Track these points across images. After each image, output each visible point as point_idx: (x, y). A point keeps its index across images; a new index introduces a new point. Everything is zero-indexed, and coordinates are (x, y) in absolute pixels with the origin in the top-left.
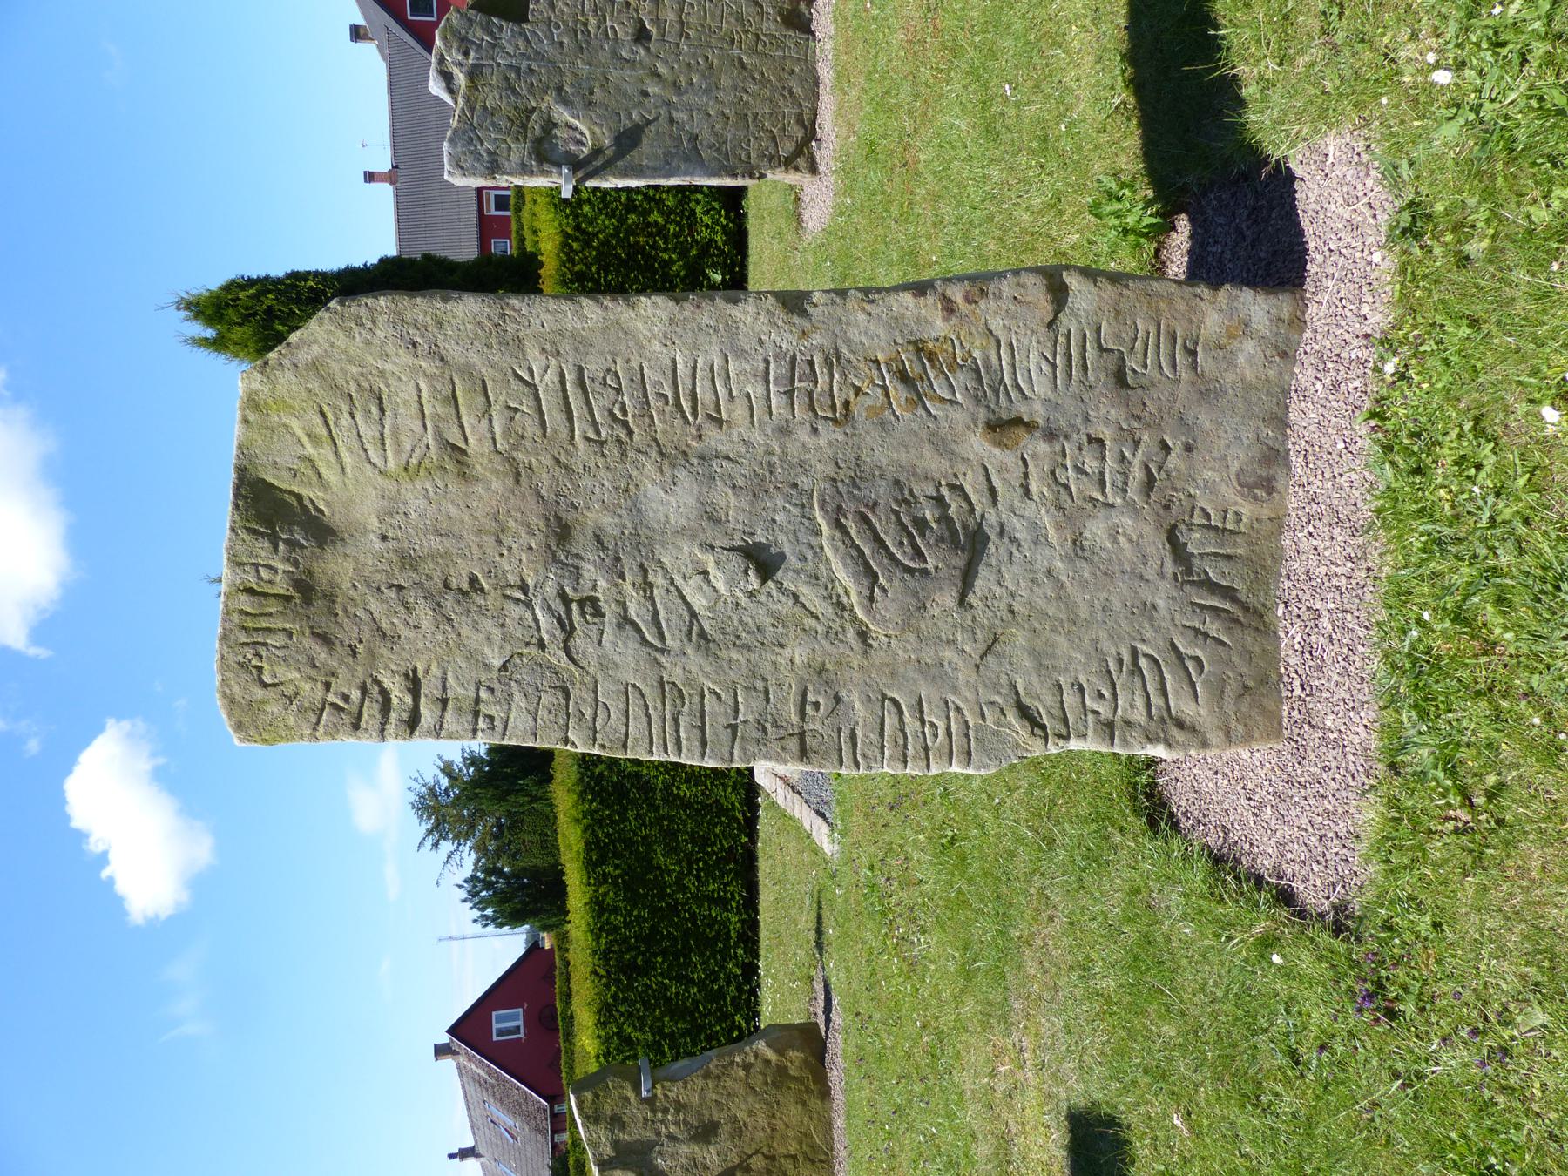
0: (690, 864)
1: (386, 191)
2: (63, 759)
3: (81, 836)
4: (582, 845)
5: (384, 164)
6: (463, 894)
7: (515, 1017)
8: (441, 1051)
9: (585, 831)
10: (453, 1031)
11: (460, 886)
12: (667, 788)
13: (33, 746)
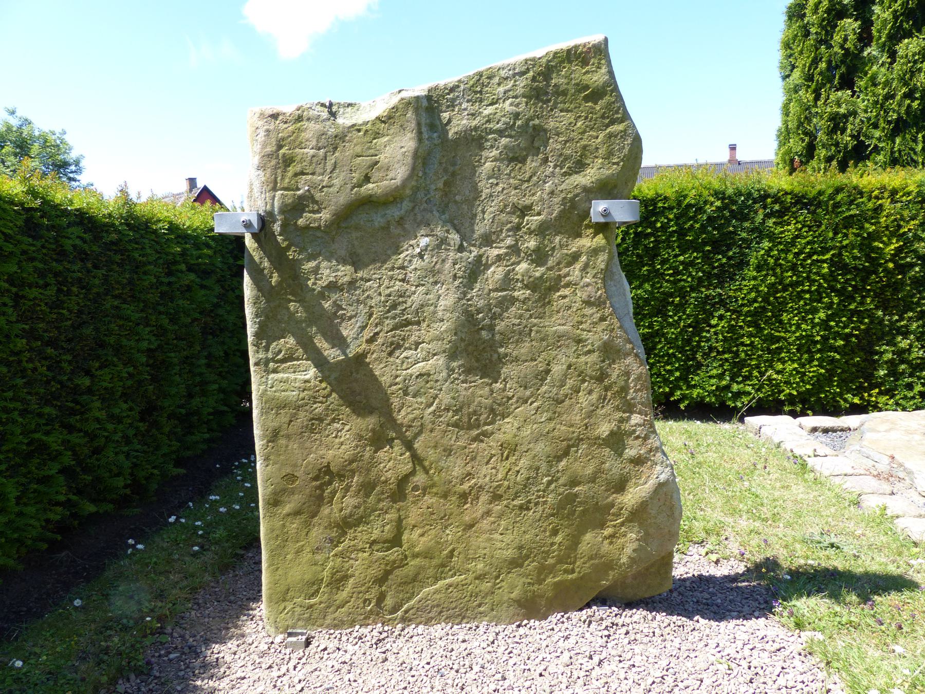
1: (723, 156)
5: (741, 156)
8: (192, 182)
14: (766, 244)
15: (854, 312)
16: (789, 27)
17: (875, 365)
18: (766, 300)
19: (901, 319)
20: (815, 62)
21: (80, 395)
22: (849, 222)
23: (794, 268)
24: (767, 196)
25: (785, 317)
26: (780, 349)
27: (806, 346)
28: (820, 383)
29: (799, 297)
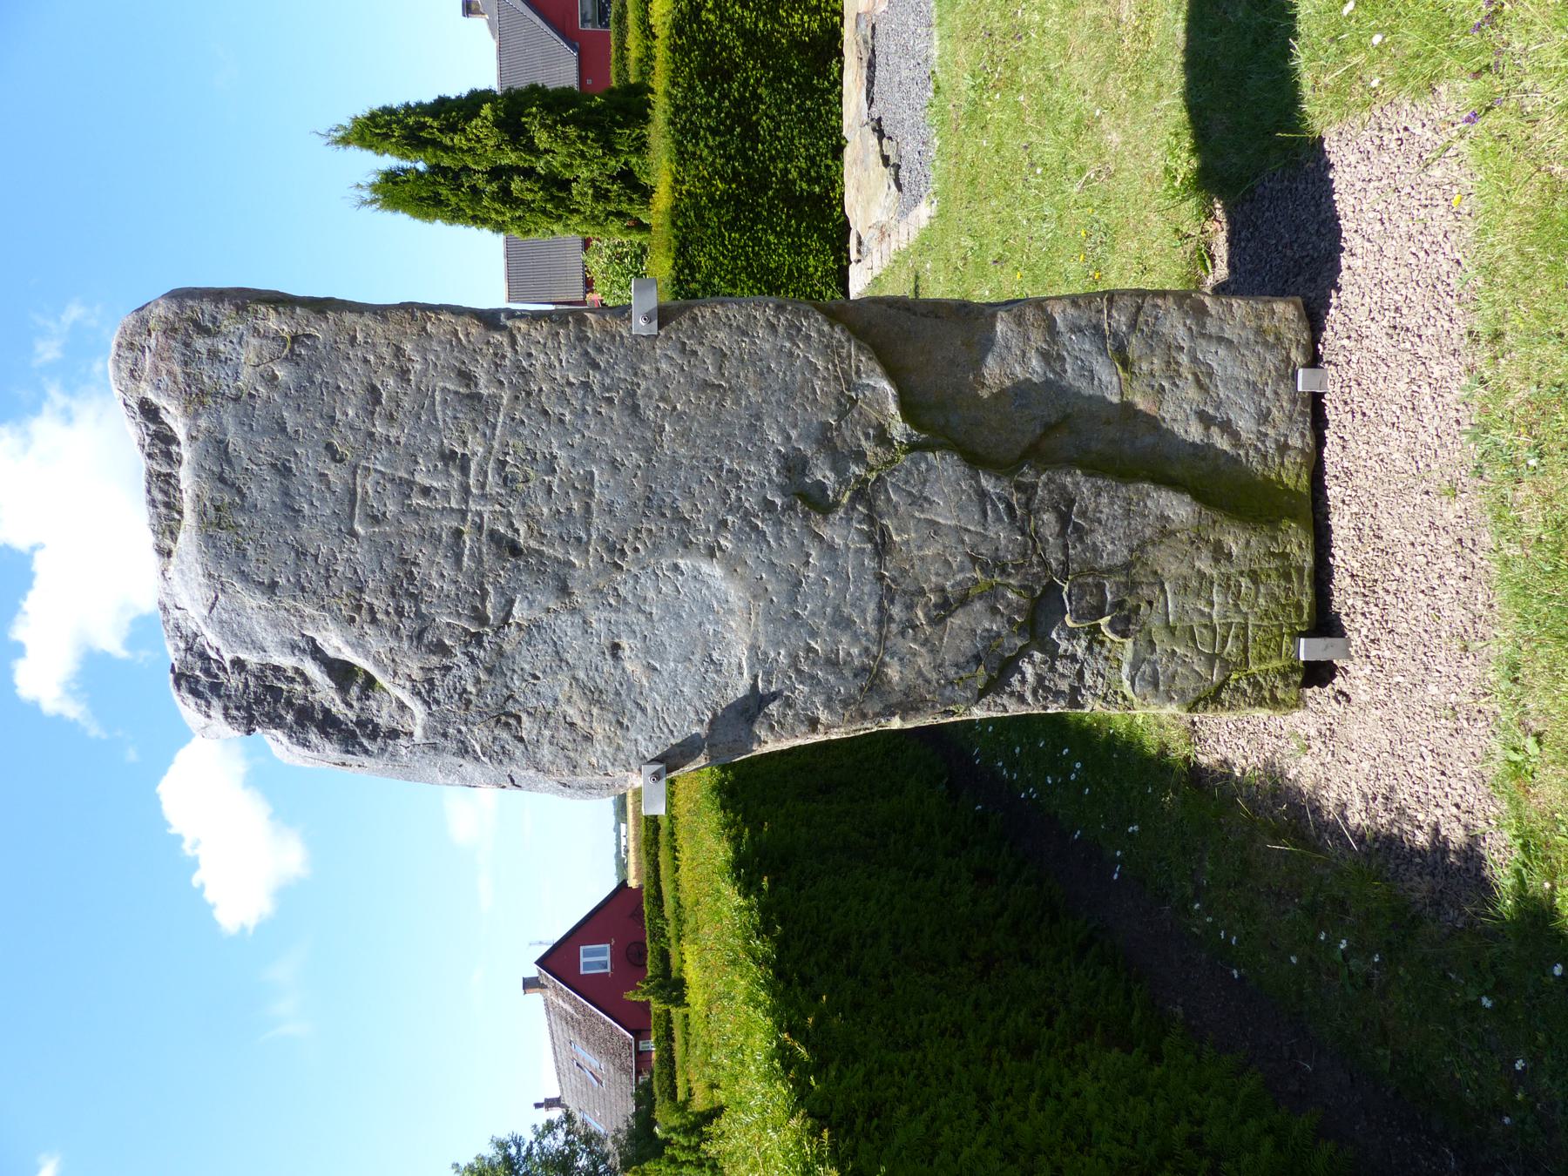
2: (159, 763)
3: (459, 98)
7: (602, 953)
8: (529, 984)
10: (541, 962)
13: (132, 755)
14: (716, 281)
15: (769, 211)
17: (811, 194)
18: (759, 281)
19: (775, 175)
20: (544, 212)
21: (839, 1070)
22: (700, 217)
23: (734, 259)
24: (678, 279)
25: (773, 265)
26: (799, 269)
27: (795, 249)
28: (825, 237)
29: (757, 254)
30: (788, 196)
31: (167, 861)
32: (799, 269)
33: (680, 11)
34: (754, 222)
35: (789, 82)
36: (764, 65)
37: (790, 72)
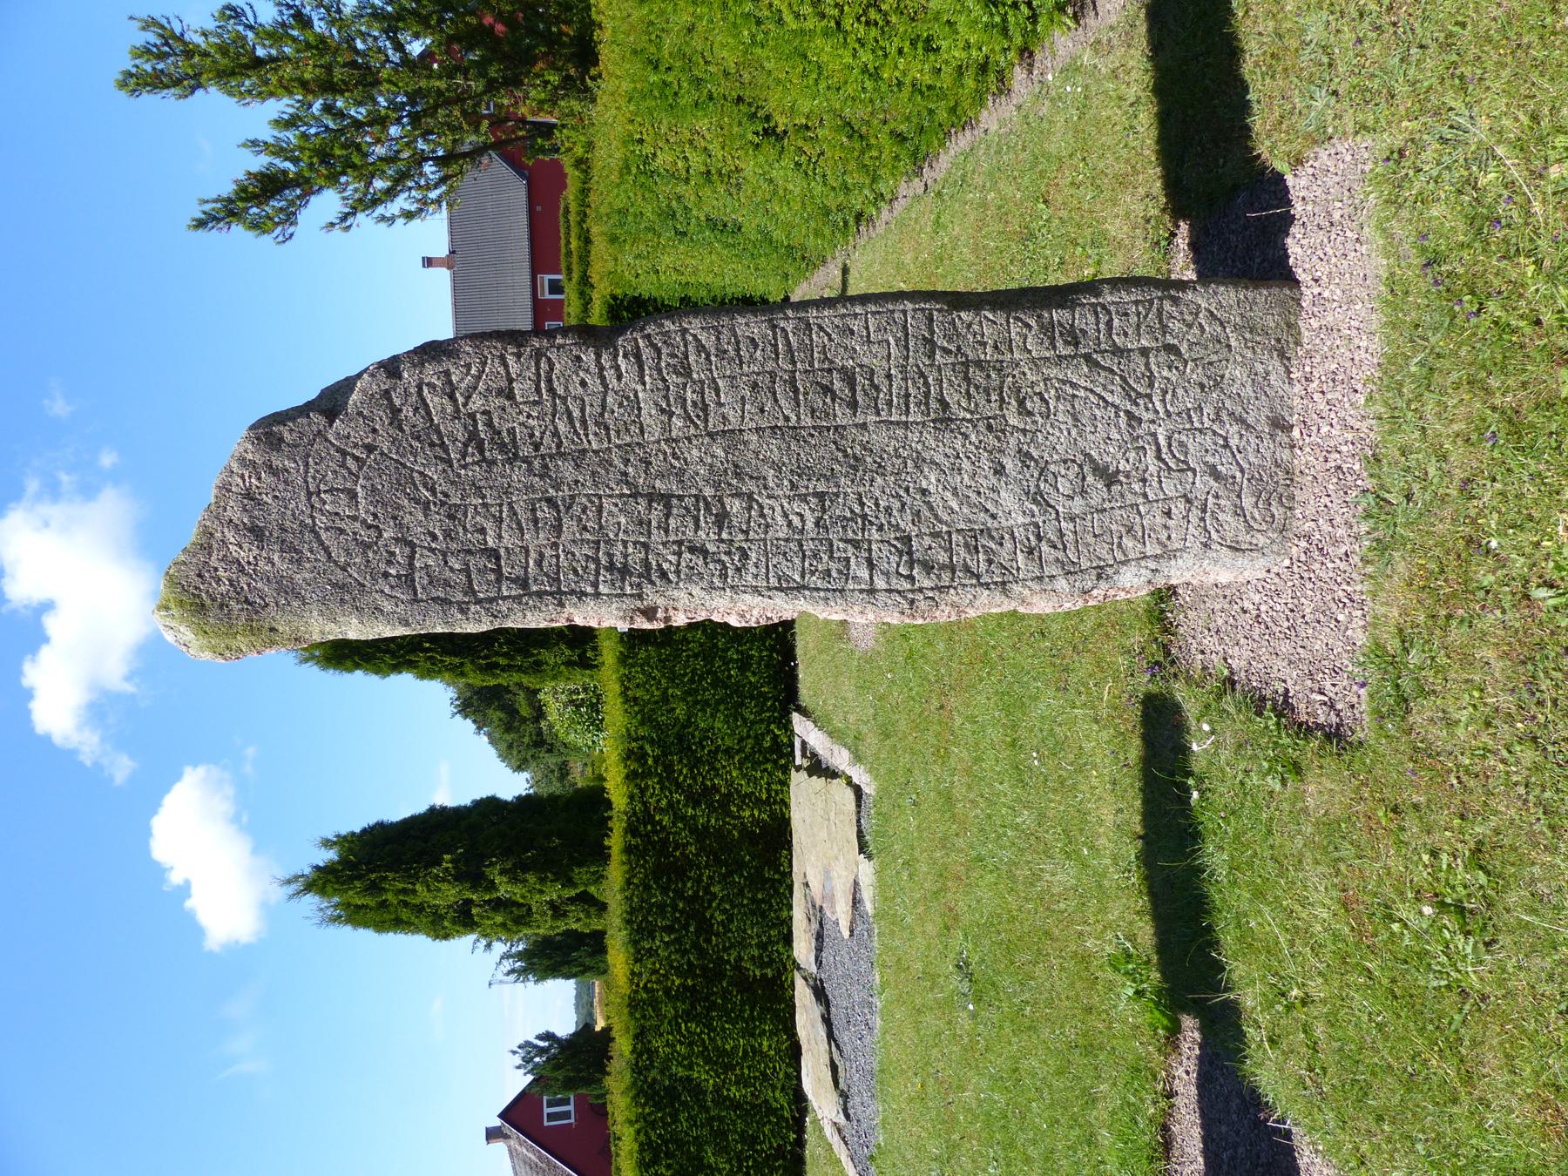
0: (740, 1161)
1: (443, 276)
4: (636, 1147)
5: (441, 249)
6: (518, 1060)
8: (492, 1134)
9: (638, 1132)
10: (502, 1116)
11: (514, 1052)
12: (717, 1089)
16: (25, 607)
18: (716, 1063)
19: (728, 962)
23: (691, 1044)
30: (744, 983)
31: (167, 904)
32: (752, 1046)
33: (635, 813)
34: (709, 1009)
35: (741, 876)
36: (717, 859)
37: (741, 865)
